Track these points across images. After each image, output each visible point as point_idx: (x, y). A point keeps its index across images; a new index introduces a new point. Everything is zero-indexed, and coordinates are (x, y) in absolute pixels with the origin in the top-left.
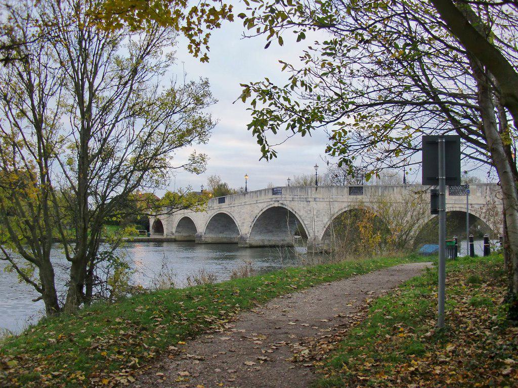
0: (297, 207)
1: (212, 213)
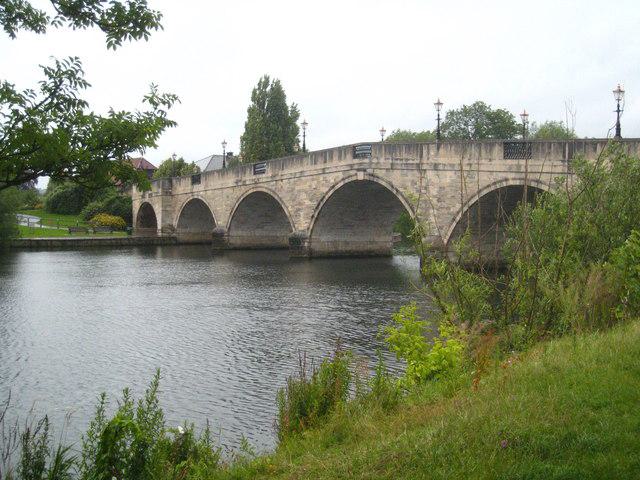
0: (399, 180)
1: (241, 193)
